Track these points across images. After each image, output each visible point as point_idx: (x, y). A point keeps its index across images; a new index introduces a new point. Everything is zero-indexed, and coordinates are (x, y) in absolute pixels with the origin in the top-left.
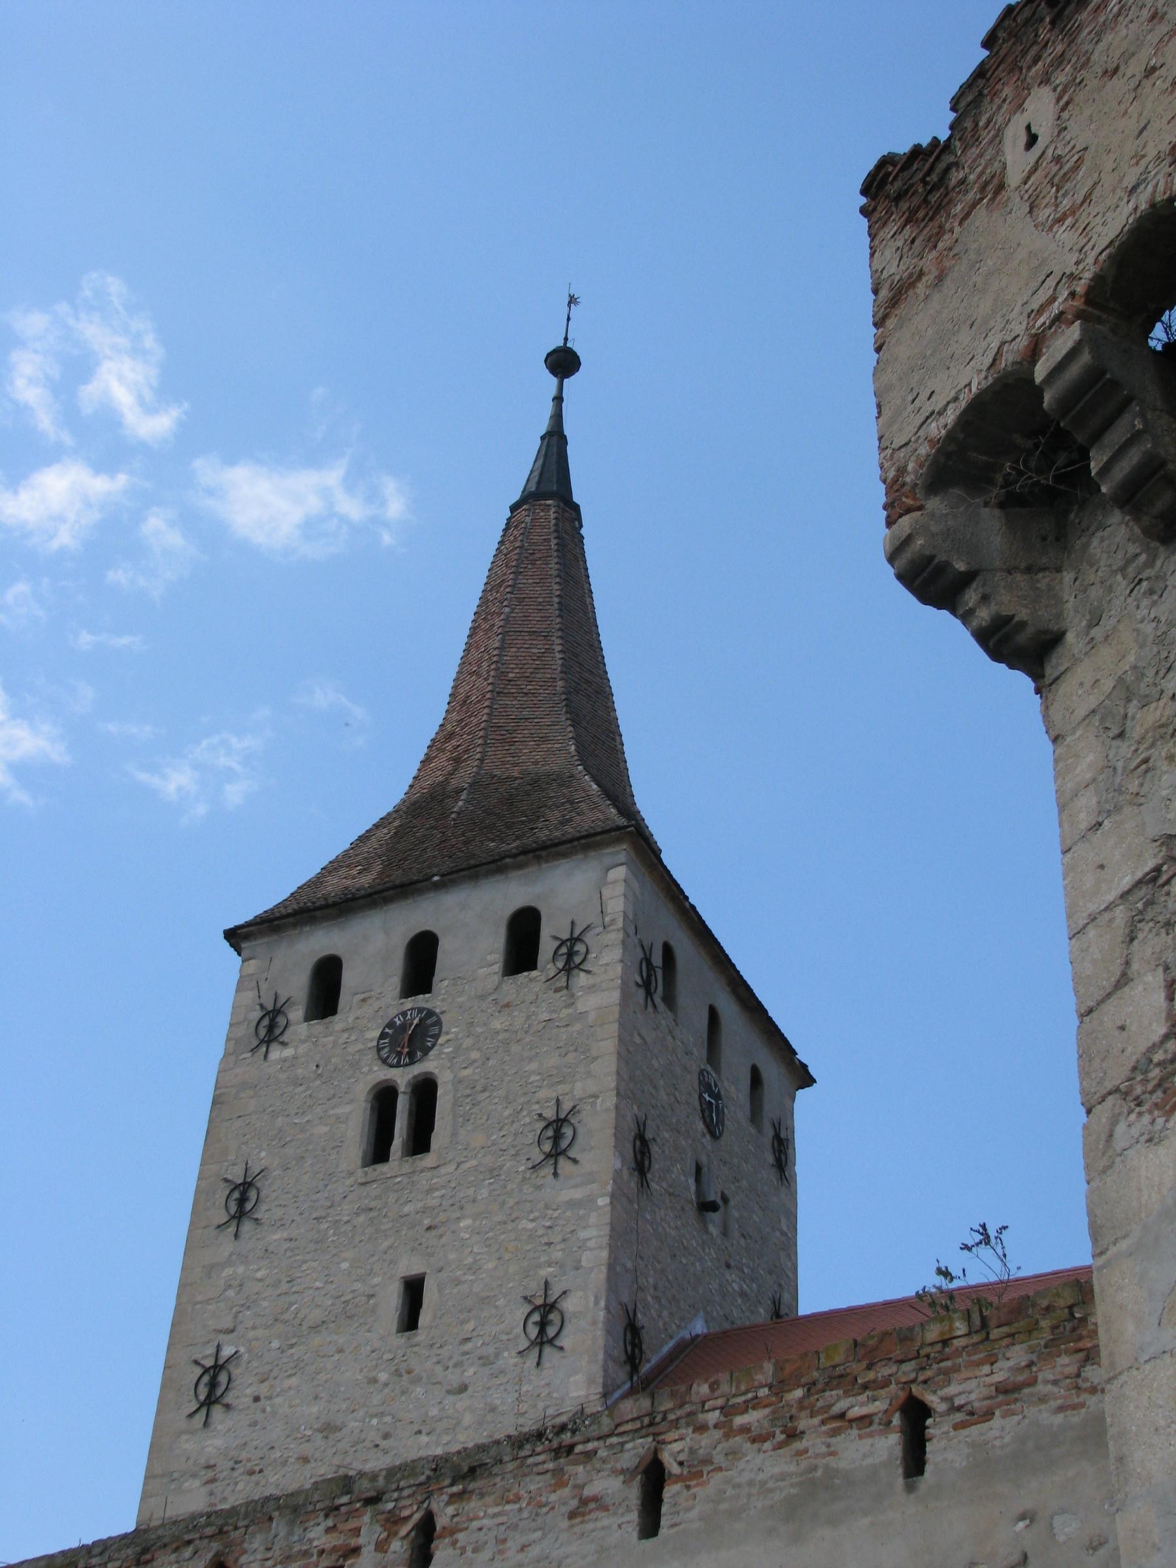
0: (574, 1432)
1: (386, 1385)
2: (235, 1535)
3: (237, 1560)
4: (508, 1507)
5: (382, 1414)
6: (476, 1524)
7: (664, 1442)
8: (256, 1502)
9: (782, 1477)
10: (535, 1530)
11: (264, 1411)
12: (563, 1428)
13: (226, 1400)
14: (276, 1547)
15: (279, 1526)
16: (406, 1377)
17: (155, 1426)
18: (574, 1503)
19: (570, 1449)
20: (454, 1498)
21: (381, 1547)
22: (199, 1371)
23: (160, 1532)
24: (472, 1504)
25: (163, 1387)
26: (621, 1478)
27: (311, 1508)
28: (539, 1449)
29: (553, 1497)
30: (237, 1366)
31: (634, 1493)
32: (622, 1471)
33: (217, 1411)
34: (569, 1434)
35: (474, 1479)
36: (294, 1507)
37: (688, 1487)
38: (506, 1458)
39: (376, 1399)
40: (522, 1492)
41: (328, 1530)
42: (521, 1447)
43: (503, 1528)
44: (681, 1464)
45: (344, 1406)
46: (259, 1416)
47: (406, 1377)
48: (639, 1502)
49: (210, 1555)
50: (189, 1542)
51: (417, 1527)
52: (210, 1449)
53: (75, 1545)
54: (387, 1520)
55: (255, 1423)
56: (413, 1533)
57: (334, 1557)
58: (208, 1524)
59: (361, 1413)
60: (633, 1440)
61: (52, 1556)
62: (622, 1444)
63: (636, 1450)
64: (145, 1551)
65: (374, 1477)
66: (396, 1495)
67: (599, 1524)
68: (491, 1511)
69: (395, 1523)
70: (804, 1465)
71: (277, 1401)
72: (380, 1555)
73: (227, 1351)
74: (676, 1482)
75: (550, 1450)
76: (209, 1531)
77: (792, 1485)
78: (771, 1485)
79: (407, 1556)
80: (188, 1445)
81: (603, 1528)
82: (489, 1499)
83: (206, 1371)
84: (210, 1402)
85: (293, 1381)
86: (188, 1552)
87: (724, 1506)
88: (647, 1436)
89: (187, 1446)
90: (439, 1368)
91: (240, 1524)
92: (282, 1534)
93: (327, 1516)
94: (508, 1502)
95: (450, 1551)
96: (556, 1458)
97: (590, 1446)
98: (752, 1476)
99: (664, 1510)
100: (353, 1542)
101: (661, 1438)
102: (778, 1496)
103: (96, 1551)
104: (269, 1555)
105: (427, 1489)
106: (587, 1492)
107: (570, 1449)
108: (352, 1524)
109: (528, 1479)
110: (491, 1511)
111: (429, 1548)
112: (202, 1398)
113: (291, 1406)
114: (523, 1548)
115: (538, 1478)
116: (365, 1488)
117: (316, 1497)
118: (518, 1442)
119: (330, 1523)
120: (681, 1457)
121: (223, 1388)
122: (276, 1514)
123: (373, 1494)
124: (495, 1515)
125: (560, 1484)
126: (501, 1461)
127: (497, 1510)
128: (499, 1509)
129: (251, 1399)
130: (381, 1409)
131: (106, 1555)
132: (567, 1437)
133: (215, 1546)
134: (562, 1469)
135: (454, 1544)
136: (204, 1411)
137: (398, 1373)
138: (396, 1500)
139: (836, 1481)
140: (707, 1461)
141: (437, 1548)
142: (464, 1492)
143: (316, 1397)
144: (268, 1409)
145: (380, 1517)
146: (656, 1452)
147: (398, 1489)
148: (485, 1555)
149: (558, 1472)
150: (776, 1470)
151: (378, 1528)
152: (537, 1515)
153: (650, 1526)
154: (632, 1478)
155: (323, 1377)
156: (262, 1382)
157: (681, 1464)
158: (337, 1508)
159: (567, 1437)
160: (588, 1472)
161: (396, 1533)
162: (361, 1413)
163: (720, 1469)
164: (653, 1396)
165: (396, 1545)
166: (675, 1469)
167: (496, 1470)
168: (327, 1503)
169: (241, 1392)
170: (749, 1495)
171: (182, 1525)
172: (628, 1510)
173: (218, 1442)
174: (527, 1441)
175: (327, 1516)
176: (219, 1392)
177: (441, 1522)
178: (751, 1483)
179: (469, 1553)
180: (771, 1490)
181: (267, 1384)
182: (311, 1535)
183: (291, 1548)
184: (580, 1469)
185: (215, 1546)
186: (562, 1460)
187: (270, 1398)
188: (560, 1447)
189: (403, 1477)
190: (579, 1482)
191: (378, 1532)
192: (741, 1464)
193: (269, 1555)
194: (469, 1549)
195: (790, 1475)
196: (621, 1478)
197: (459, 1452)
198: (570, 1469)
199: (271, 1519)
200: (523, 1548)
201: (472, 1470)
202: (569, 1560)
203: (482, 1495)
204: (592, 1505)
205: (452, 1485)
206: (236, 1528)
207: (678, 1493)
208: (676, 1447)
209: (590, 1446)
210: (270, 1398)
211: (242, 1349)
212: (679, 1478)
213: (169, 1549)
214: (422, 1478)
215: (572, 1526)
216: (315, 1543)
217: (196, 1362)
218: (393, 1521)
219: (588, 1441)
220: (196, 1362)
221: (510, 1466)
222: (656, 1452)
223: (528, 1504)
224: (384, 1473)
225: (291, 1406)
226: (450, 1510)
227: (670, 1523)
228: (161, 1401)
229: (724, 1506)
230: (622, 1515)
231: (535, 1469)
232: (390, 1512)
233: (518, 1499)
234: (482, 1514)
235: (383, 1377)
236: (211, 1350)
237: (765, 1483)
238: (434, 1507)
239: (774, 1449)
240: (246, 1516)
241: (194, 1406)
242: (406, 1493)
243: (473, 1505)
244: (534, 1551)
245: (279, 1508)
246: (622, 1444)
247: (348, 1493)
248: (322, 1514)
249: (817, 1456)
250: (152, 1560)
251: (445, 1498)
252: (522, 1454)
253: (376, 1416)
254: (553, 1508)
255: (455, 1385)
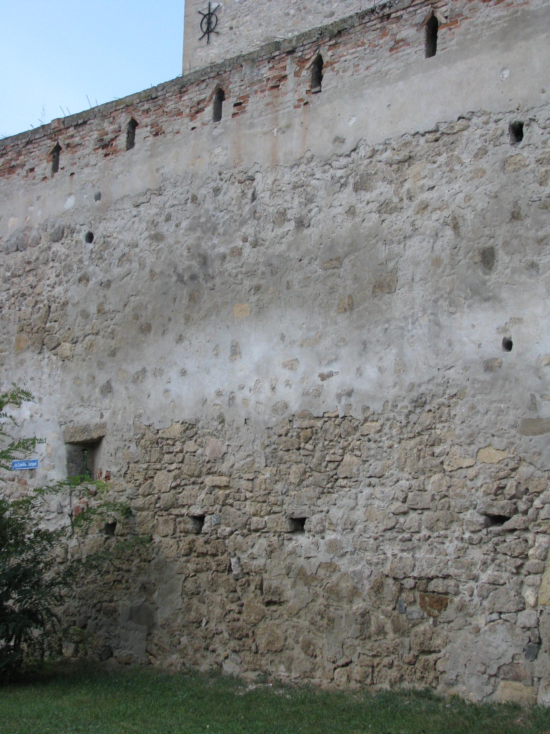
0: (390, 7)
1: (294, 16)
2: (225, 75)
3: (227, 87)
4: (359, 49)
5: (293, 30)
6: (343, 59)
7: (437, 7)
8: (233, 59)
9: (499, 18)
10: (373, 58)
11: (235, 34)
12: (384, 6)
13: (216, 30)
14: (246, 79)
15: (246, 69)
16: (303, 11)
17: (184, 45)
18: (392, 43)
19: (389, 16)
20: (331, 47)
21: (297, 74)
22: (201, 17)
23: (189, 77)
24: (341, 49)
25: (185, 26)
26: (416, 28)
27: (260, 59)
28: (373, 18)
29: (381, 42)
30: (220, 12)
31: (422, 35)
32: (416, 25)
33: (213, 36)
34: (388, 9)
35: (341, 37)
36: (253, 60)
37: (450, 29)
38: (356, 25)
39: (290, 23)
40: (365, 41)
41: (270, 69)
42: (363, 18)
43: (357, 59)
44: (446, 17)
45: (274, 28)
46: (234, 37)
47: (303, 11)
48: (425, 39)
49: (215, 86)
50: (203, 81)
51: (314, 63)
52: (211, 55)
53: (150, 87)
54: (299, 61)
55: (232, 40)
56: (312, 67)
57: (275, 81)
58: (212, 72)
59: (283, 31)
60: (421, 8)
61: (140, 93)
62: (415, 11)
63: (423, 13)
64: (183, 87)
65: (291, 41)
66: (302, 48)
67: (405, 53)
68: (350, 51)
69: (303, 62)
70: (511, 10)
71: (242, 28)
72: (297, 78)
73: (214, 6)
74: (444, 27)
75: (378, 18)
76: (212, 75)
77: (505, 22)
78: (493, 23)
79: (310, 77)
80: (201, 53)
81: (408, 54)
82: (349, 46)
83: (205, 16)
84: (209, 32)
85: (248, 18)
86: (203, 86)
87: (469, 37)
88: (428, 5)
89: (200, 54)
90: (320, 5)
91: (227, 70)
92: (248, 73)
93: (269, 62)
94: (359, 46)
95: (331, 73)
96: (382, 22)
97: (399, 14)
98: (484, 19)
99: (438, 42)
100: (283, 73)
101: (435, 5)
102: (497, 28)
103: (160, 89)
104: (243, 83)
105: (317, 44)
106: (398, 37)
107: (389, 16)
108: (282, 65)
109: (368, 34)
110: (350, 51)
111: (321, 72)
112: (205, 30)
113: (248, 31)
114: (367, 68)
115: (373, 33)
116: (287, 47)
117: (263, 54)
118: (362, 16)
119: (271, 65)
120: (446, 14)
121: (214, 24)
122: (244, 64)
123: (290, 49)
124: (352, 53)
125: (384, 35)
126: (354, 27)
127: (354, 50)
128: (354, 50)
129: (228, 29)
130: (292, 28)
131: (165, 91)
132: (387, 11)
133: (216, 81)
134: (385, 27)
135: (333, 69)
136: (206, 36)
137: (299, 10)
138: (302, 51)
139: (528, 17)
140: (460, 15)
141: (325, 72)
142: (336, 43)
143: (260, 25)
144: (237, 33)
145: (295, 60)
146: (433, 13)
147: (303, 45)
148: (349, 73)
149: (383, 29)
150: (496, 15)
151: (295, 66)
152: (374, 51)
153: (431, 50)
154: (421, 28)
155: (262, 14)
156: (233, 20)
157: (446, 17)
158: (274, 58)
159: (387, 11)
160: (399, 27)
161: (304, 67)
162: (283, 31)
163: (467, 18)
164: (337, 585)
165: (304, 73)
166: (443, 21)
167: (351, 31)
168: (269, 56)
169: (224, 23)
170: (482, 30)
171: (199, 73)
172: (420, 44)
173: (215, 51)
174: (366, 14)
175: (269, 62)
176: (212, 27)
177: (325, 59)
178: (483, 23)
179: (341, 73)
180: (494, 26)
181: (235, 20)
182: (263, 72)
183: (253, 79)
184: (394, 26)
185: (216, 81)
186: (385, 23)
187: (237, 27)
188: (383, 16)
189: (305, 39)
190: (394, 32)
191: (295, 68)
192: (478, 14)
193: (243, 83)
194: (341, 71)
195: (504, 17)
196: (416, 28)
197: (332, 24)
198: (389, 27)
199: (242, 66)
200: (367, 68)
201: (339, 32)
202: (391, 71)
203: (345, 44)
204: (401, 44)
205: (330, 40)
206: (225, 72)
207: (445, 33)
208: (444, 9)
209: (399, 14)
210: (237, 27)
211: (221, 4)
212: (446, 25)
213: (194, 85)
214: (315, 39)
215: (392, 55)
216: (265, 76)
217: (200, 12)
218: (302, 61)
219: (398, 11)
220: (200, 12)
221: (359, 28)
222: (433, 13)
223: (369, 46)
224: (295, 39)
225: (248, 31)
226: (330, 53)
227: (441, 48)
228: (185, 33)
229: (469, 37)
230: (417, 46)
231: (371, 28)
232: (300, 57)
233: (363, 44)
234: (345, 53)
235: (292, 12)
236: (206, 6)
237: (491, 22)
238: (322, 52)
239: (495, 4)
240: (229, 66)
241: (201, 34)
242: (307, 47)
243: (341, 49)
244: (373, 69)
245: (245, 60)
246: (415, 11)
247: (278, 50)
248: (266, 62)
249: (518, 5)
250: (187, 91)
251: (327, 47)
252: (364, 21)
253: (290, 32)
254: (381, 47)
255: (328, 13)
